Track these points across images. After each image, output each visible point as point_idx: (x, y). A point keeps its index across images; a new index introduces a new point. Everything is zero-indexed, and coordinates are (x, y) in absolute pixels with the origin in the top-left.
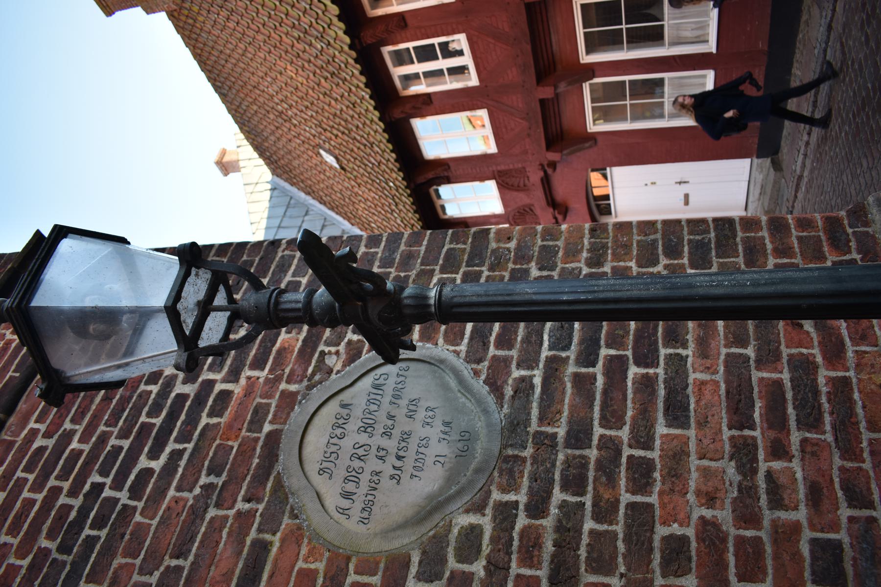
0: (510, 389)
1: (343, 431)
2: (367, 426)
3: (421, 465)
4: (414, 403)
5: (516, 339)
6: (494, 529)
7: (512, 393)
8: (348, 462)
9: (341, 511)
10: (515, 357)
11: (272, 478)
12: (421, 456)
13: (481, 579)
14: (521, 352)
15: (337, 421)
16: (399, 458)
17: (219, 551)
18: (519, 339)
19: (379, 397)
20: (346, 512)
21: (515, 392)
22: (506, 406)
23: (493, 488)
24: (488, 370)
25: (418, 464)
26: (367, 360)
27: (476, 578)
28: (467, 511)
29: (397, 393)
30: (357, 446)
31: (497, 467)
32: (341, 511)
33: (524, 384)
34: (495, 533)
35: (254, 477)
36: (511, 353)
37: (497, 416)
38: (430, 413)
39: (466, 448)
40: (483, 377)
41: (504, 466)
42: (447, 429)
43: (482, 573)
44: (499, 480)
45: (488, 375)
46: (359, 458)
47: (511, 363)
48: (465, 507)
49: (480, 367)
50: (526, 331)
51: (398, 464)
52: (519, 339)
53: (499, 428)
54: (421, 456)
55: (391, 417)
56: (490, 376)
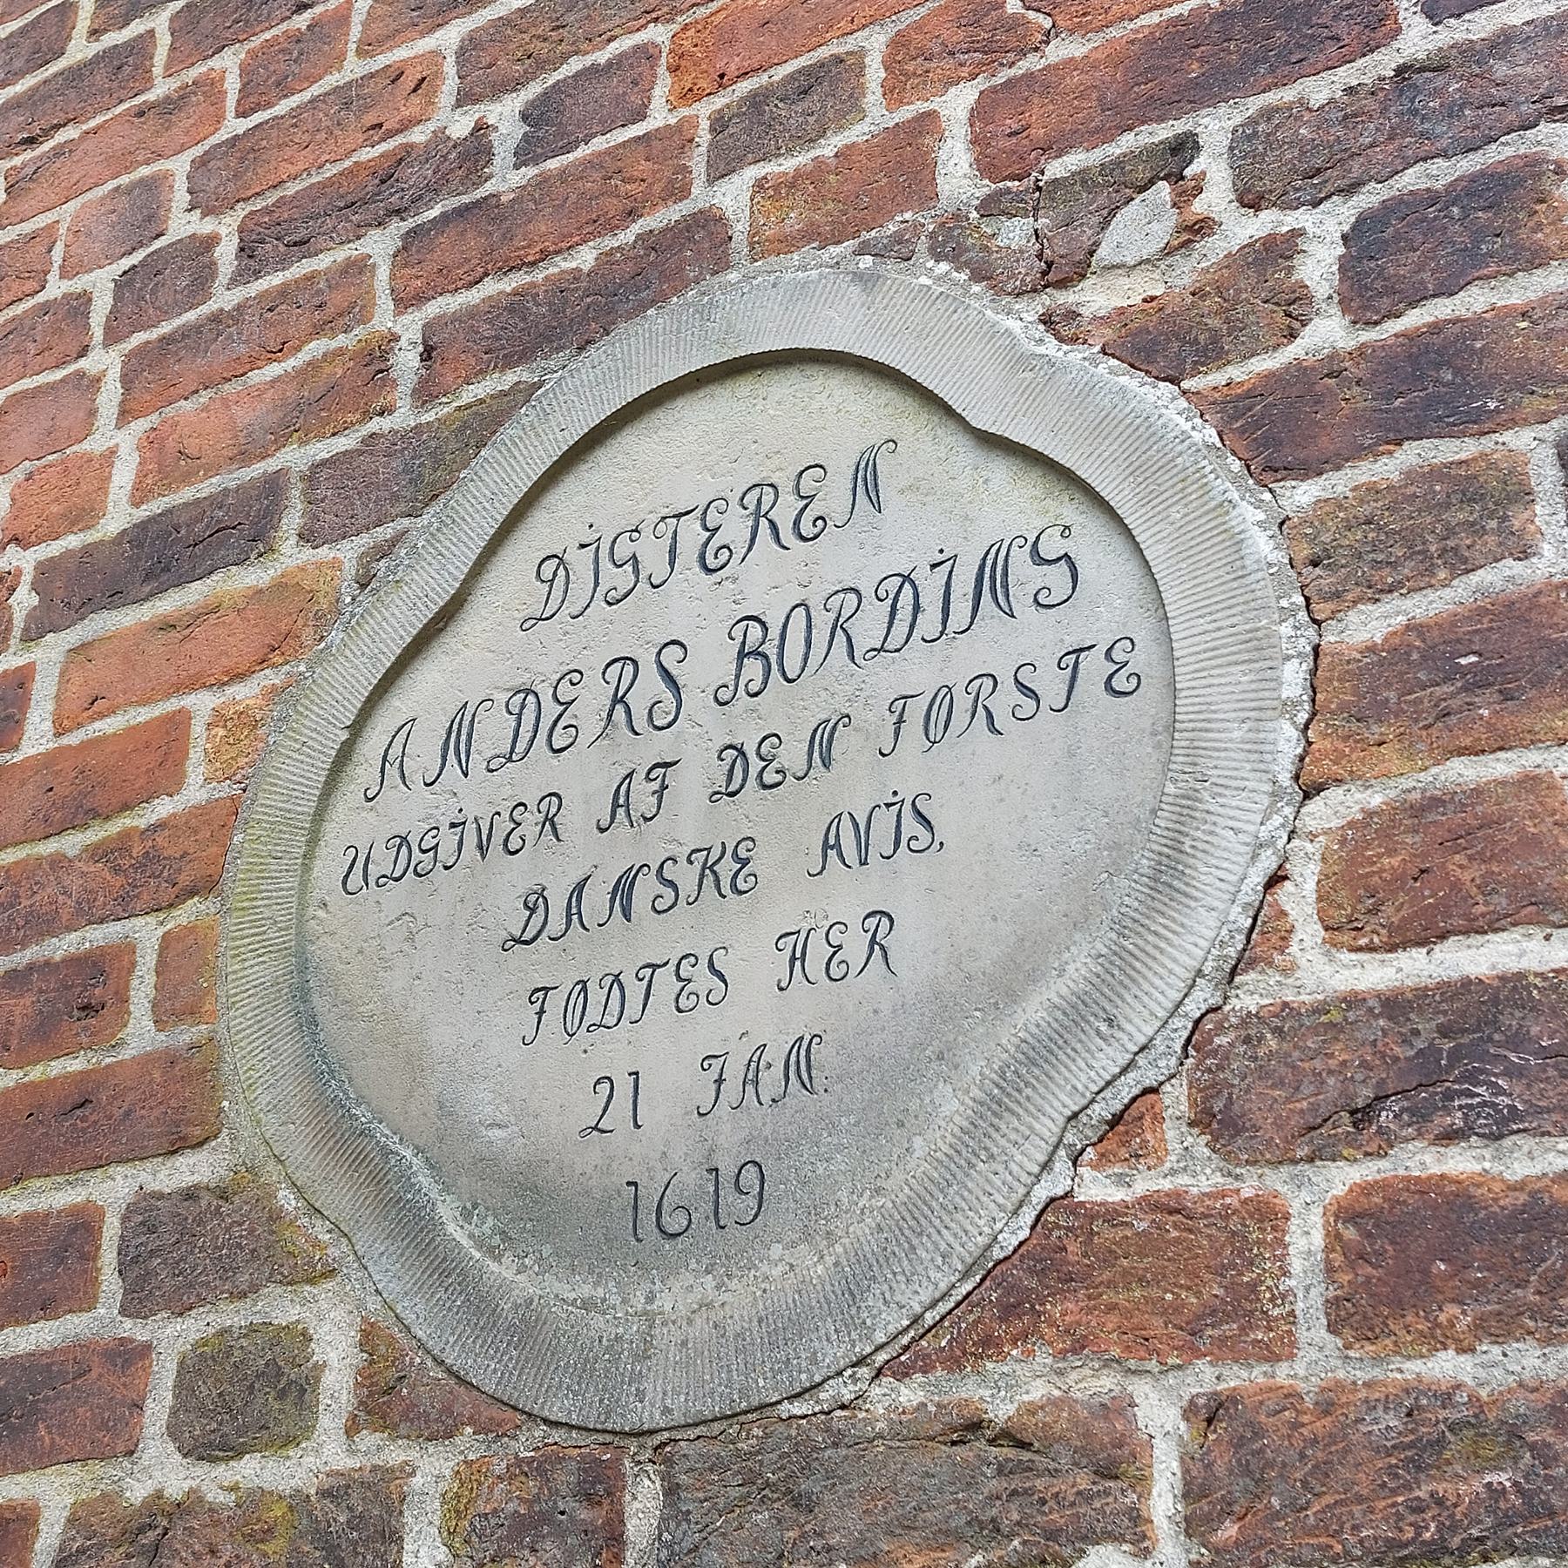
0: (1038, 1391)
1: (740, 551)
2: (770, 649)
3: (593, 1015)
4: (910, 826)
5: (1438, 1339)
6: (297, 1502)
7: (1001, 1411)
8: (592, 663)
9: (396, 751)
10: (1283, 1373)
11: (511, 378)
12: (635, 991)
13: (120, 1494)
14: (1326, 1408)
15: (1006, 682)
16: (623, 891)
17: (255, 377)
18: (1445, 1366)
19: (929, 621)
20: (392, 772)
21: (1009, 1437)
22: (910, 1394)
23: (468, 1442)
24: (1152, 1204)
25: (596, 995)
26: (1145, 431)
27: (112, 1470)
28: (369, 1337)
29: (963, 703)
30: (671, 656)
31: (557, 1435)
32: (396, 751)
33: (1084, 1481)
34: (278, 1511)
35: (516, 304)
36: (1314, 1334)
37: (836, 1353)
38: (855, 947)
39: (674, 1223)
40: (1097, 1188)
41: (565, 1478)
42: (771, 1080)
43: (137, 1492)
44: (500, 1468)
45: (1112, 1214)
46: (618, 700)
47: (1227, 1351)
48: (387, 1322)
49: (1175, 1136)
50: (1519, 1405)
51: (596, 899)
52: (1445, 1366)
53: (764, 1388)
54: (635, 991)
55: (822, 747)
56: (1107, 1234)
